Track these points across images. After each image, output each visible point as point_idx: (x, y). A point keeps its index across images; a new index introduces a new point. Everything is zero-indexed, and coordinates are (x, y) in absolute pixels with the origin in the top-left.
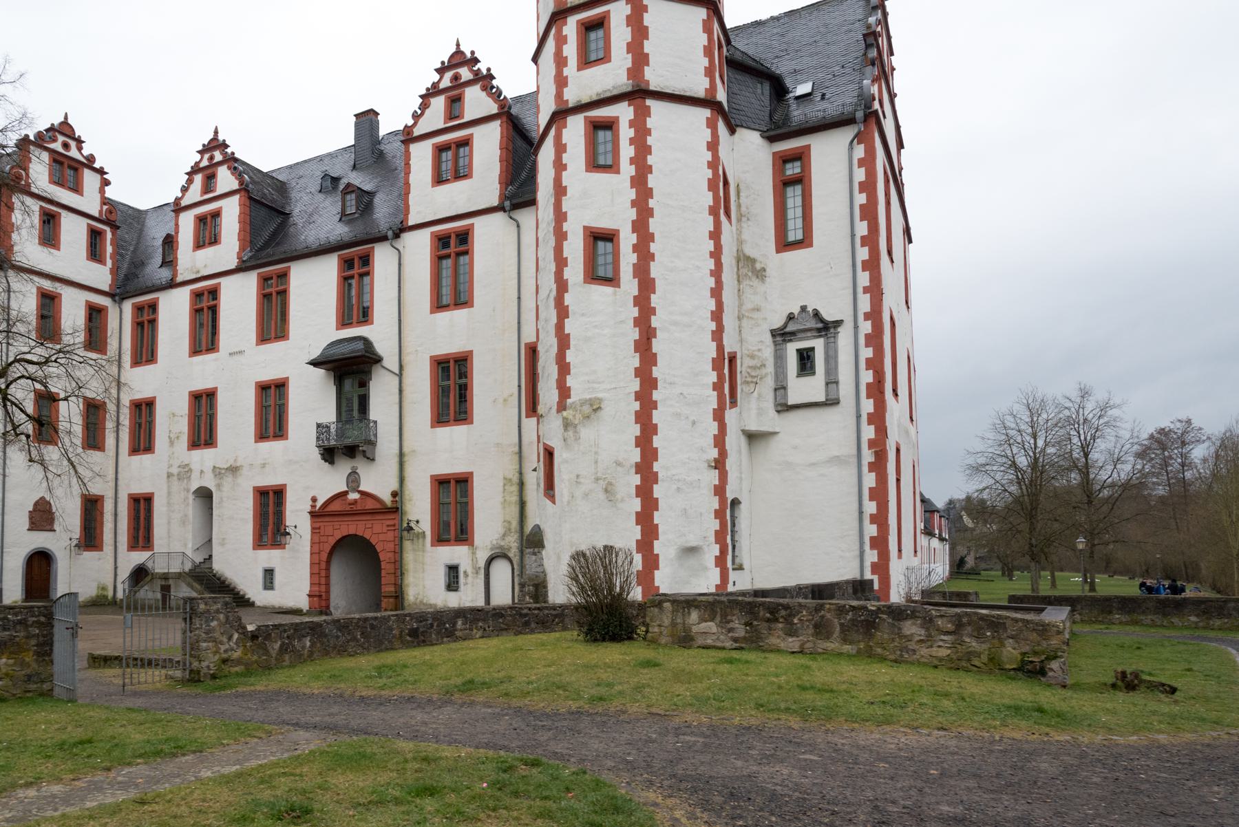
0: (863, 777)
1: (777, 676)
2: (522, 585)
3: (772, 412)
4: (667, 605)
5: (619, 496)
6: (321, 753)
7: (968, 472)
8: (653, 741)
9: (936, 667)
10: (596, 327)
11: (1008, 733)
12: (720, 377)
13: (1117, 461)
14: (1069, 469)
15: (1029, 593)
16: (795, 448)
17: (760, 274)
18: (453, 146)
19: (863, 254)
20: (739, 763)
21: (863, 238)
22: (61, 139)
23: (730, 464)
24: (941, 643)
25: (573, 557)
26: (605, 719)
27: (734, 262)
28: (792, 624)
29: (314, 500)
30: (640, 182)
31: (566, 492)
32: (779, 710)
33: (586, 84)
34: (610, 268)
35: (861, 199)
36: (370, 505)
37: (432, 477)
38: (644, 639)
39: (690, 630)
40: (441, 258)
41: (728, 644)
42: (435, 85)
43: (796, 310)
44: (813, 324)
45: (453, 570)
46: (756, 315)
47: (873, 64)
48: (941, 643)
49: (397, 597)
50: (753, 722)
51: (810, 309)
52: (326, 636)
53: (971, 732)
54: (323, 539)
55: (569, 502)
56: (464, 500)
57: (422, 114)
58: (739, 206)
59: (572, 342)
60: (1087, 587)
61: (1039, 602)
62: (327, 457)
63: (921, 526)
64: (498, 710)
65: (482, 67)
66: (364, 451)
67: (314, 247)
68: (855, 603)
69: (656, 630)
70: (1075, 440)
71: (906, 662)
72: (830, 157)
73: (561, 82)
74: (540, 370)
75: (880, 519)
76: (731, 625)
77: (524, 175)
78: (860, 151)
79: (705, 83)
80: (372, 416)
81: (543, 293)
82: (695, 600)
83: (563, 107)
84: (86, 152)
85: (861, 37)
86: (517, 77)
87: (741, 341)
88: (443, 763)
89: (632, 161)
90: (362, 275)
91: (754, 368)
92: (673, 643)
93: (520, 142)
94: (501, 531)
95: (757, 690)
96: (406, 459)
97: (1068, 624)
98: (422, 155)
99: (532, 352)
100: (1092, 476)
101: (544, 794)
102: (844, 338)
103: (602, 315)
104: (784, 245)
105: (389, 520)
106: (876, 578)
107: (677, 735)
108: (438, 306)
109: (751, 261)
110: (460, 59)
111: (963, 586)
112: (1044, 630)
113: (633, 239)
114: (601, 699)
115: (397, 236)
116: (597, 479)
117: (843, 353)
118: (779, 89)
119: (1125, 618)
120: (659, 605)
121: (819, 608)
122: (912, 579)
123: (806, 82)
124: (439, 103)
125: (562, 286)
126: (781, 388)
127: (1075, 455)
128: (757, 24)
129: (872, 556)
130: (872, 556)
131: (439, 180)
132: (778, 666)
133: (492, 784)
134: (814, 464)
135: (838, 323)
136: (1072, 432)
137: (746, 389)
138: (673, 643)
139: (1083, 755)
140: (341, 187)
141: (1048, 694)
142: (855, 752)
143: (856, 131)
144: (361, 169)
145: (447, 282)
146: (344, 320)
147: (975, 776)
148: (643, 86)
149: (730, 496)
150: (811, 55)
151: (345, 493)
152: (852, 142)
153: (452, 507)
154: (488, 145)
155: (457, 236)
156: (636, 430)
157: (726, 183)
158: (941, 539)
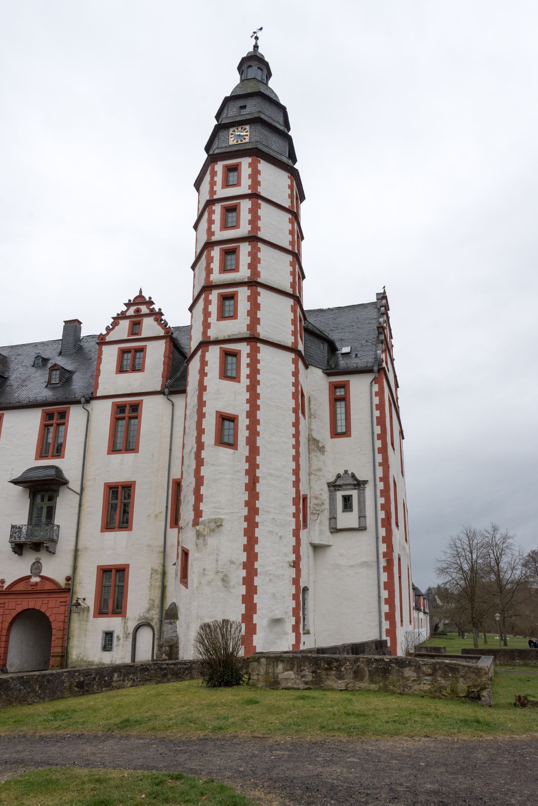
0: (384, 770)
1: (332, 707)
2: (160, 646)
3: (328, 533)
4: (263, 660)
5: (231, 584)
6: (16, 782)
7: (438, 572)
8: (256, 756)
9: (423, 697)
10: (221, 473)
11: (462, 737)
12: (298, 509)
13: (513, 569)
14: (489, 573)
15: (472, 647)
16: (341, 555)
17: (322, 450)
18: (133, 351)
19: (378, 444)
20: (311, 767)
21: (378, 435)
23: (303, 564)
24: (425, 682)
25: (201, 628)
26: (223, 742)
27: (306, 441)
28: (340, 671)
30: (252, 388)
31: (196, 581)
32: (334, 729)
33: (220, 329)
34: (232, 437)
35: (377, 413)
36: (48, 586)
38: (247, 684)
39: (278, 677)
40: (118, 419)
41: (302, 686)
42: (123, 313)
43: (342, 473)
44: (351, 481)
45: (109, 635)
46: (319, 473)
47: (382, 343)
48: (425, 682)
49: (62, 656)
50: (319, 739)
51: (350, 472)
52: (11, 689)
53: (442, 737)
54: (7, 612)
55: (197, 587)
56: (121, 584)
57: (113, 329)
58: (310, 409)
59: (205, 482)
60: (502, 643)
61: (474, 654)
62: (17, 550)
63: (413, 604)
64: (148, 741)
65: (156, 307)
66: (47, 547)
67: (24, 402)
68: (377, 657)
69: (255, 677)
70: (492, 556)
71: (407, 694)
72: (360, 388)
73: (206, 326)
74: (182, 498)
75: (390, 601)
76: (303, 673)
77: (178, 374)
78: (376, 388)
79: (292, 339)
80: (57, 522)
81: (187, 449)
82: (281, 656)
83: (207, 340)
85: (376, 328)
86: (178, 315)
87: (310, 488)
88: (112, 783)
89: (248, 376)
90: (58, 425)
91: (317, 505)
92: (266, 686)
93: (177, 354)
94: (147, 606)
95: (320, 717)
96: (79, 553)
97: (493, 667)
98: (110, 356)
99: (178, 485)
100: (501, 577)
101: (187, 798)
102: (369, 491)
104: (335, 434)
105: (62, 598)
106: (388, 639)
107: (271, 751)
108: (113, 449)
109: (316, 441)
111: (438, 643)
112: (478, 671)
113: (247, 422)
114: (220, 728)
115: (88, 401)
116: (217, 572)
117: (368, 498)
118: (333, 348)
119: (522, 662)
120: (258, 660)
121: (356, 660)
122: (409, 639)
123: (347, 346)
124: (125, 324)
126: (333, 518)
127: (492, 565)
128: (321, 311)
130: (386, 625)
131: (121, 370)
132: (333, 700)
133: (149, 795)
134: (352, 566)
135: (365, 482)
136: (491, 551)
137: (313, 517)
138: (266, 686)
139: (499, 748)
140: (49, 365)
141: (482, 711)
142: (379, 754)
143: (374, 377)
144: (65, 356)
145: (121, 434)
146: (41, 454)
147: (444, 764)
148: (256, 336)
149: (302, 585)
150: (350, 332)
152: (372, 382)
153: (112, 589)
154: (156, 354)
155: (131, 406)
156: (244, 540)
157: (303, 395)
158: (425, 613)
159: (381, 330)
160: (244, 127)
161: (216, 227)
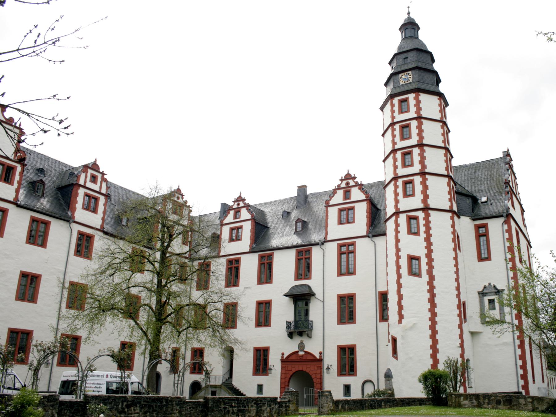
12: (460, 312)
22: (177, 195)
29: (283, 354)
30: (428, 239)
33: (406, 204)
36: (309, 358)
37: (338, 346)
42: (339, 186)
43: (487, 284)
44: (494, 290)
51: (492, 284)
65: (358, 180)
72: (495, 228)
75: (524, 367)
84: (184, 200)
89: (425, 232)
93: (374, 209)
98: (333, 213)
103: (415, 289)
110: (348, 177)
113: (426, 260)
115: (323, 244)
118: (475, 200)
124: (340, 193)
125: (399, 276)
129: (522, 382)
130: (522, 382)
131: (340, 223)
135: (503, 290)
145: (344, 263)
146: (298, 277)
149: (466, 358)
151: (297, 352)
154: (361, 212)
156: (430, 332)
159: (507, 185)
160: (408, 72)
161: (397, 139)
